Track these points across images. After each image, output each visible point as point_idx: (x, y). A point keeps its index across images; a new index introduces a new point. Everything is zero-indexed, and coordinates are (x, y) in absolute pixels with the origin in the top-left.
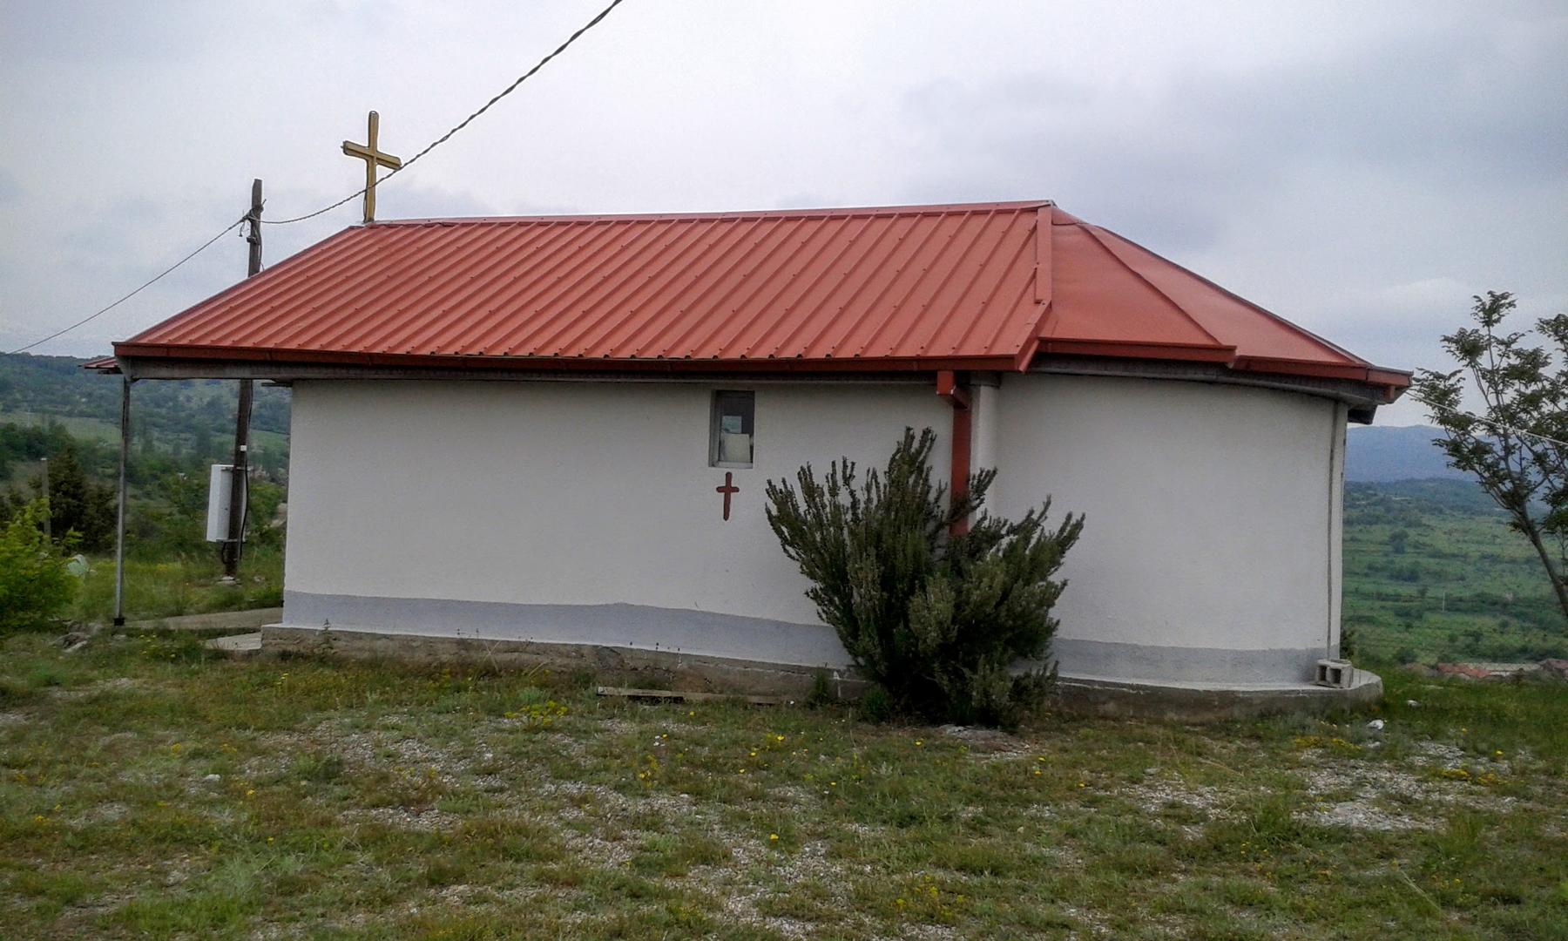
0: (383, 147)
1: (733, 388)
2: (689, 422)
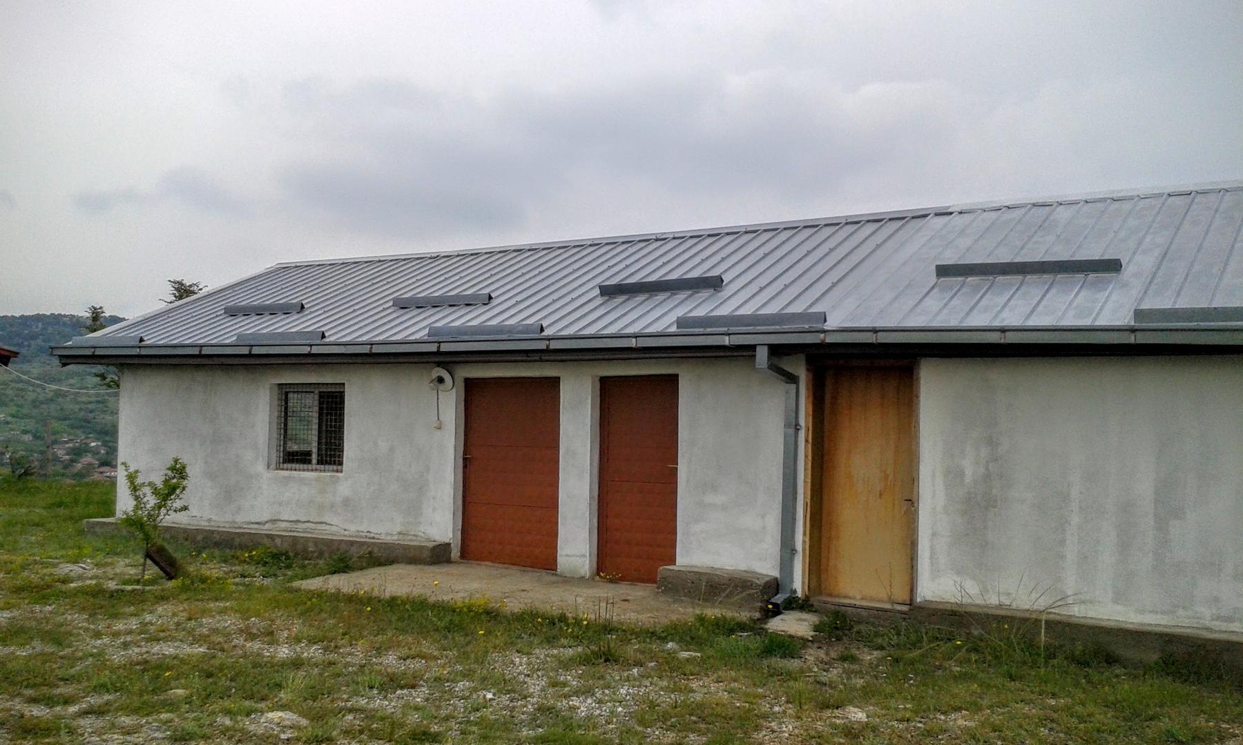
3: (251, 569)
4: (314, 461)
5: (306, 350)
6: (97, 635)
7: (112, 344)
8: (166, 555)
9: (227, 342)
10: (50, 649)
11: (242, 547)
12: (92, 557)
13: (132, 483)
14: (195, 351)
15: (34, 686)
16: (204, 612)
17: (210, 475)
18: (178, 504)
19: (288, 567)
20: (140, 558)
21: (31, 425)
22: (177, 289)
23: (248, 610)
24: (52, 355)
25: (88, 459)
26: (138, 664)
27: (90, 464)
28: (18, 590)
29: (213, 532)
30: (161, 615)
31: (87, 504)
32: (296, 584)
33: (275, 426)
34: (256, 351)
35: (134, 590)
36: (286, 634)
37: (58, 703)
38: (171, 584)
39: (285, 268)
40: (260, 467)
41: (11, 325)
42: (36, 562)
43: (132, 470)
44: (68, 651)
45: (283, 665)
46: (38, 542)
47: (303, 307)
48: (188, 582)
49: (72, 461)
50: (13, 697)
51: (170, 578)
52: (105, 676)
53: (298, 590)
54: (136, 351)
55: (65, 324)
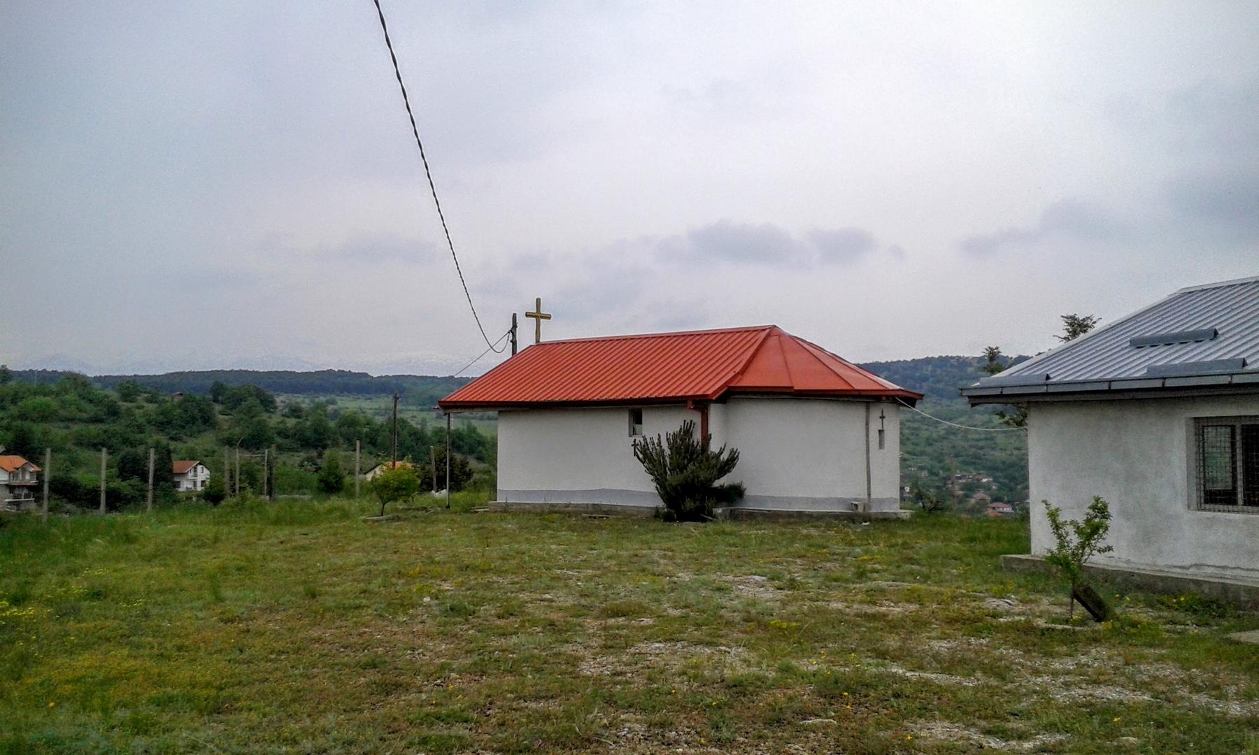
0: (543, 311)
1: (635, 409)
2: (621, 422)
3: (1180, 616)
4: (1240, 501)
5: (1225, 380)
6: (1036, 672)
7: (1013, 383)
8: (1093, 596)
9: (1137, 375)
10: (993, 682)
11: (1164, 592)
12: (1016, 593)
13: (1054, 521)
14: (1105, 387)
15: (986, 718)
16: (1142, 657)
17: (1126, 514)
18: (1101, 544)
19: (1222, 616)
20: (1067, 600)
21: (926, 461)
22: (1070, 324)
23: (1187, 659)
24: (961, 395)
25: (980, 495)
26: (1084, 706)
27: (983, 500)
28: (951, 621)
29: (1132, 574)
30: (1097, 657)
31: (999, 539)
32: (1235, 635)
33: (1193, 465)
34: (1169, 383)
35: (1063, 630)
36: (1233, 689)
37: (1013, 739)
38: (1100, 626)
39: (1190, 294)
40: (1179, 507)
41: (904, 369)
42: (963, 595)
43: (1053, 508)
44: (1010, 686)
45: (1238, 723)
46: (960, 575)
47: (1216, 333)
48: (1118, 625)
49: (966, 496)
50: (967, 727)
51: (1099, 620)
52: (1054, 716)
53: (1238, 643)
54: (1043, 390)
55: (952, 366)
